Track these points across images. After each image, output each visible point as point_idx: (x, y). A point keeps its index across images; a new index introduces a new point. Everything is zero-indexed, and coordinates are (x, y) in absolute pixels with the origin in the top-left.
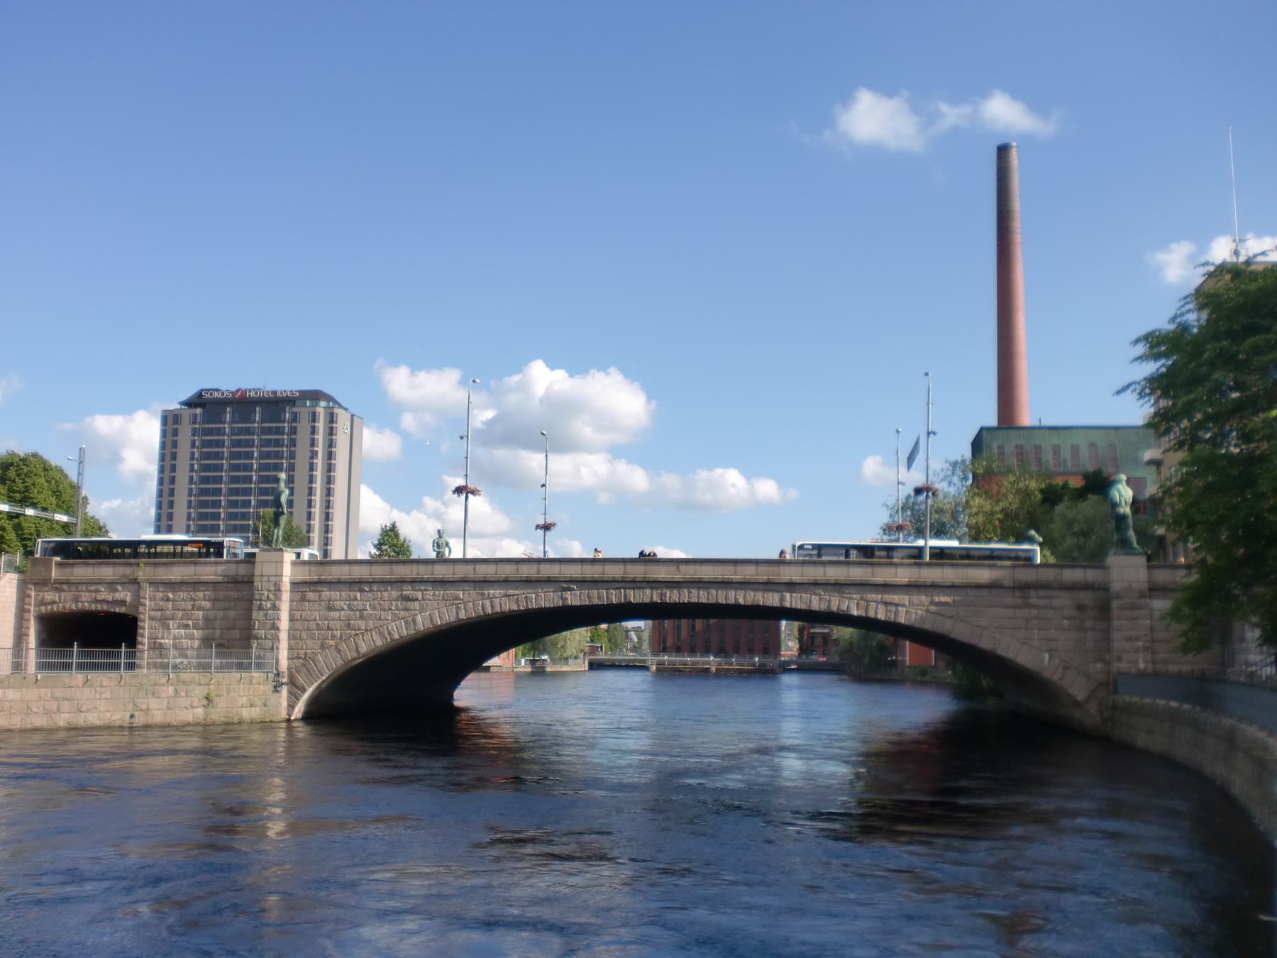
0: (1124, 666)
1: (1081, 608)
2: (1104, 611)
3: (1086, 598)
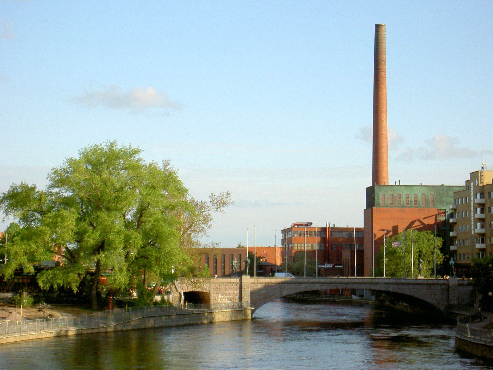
0: (452, 303)
1: (442, 289)
2: (448, 290)
3: (444, 287)
